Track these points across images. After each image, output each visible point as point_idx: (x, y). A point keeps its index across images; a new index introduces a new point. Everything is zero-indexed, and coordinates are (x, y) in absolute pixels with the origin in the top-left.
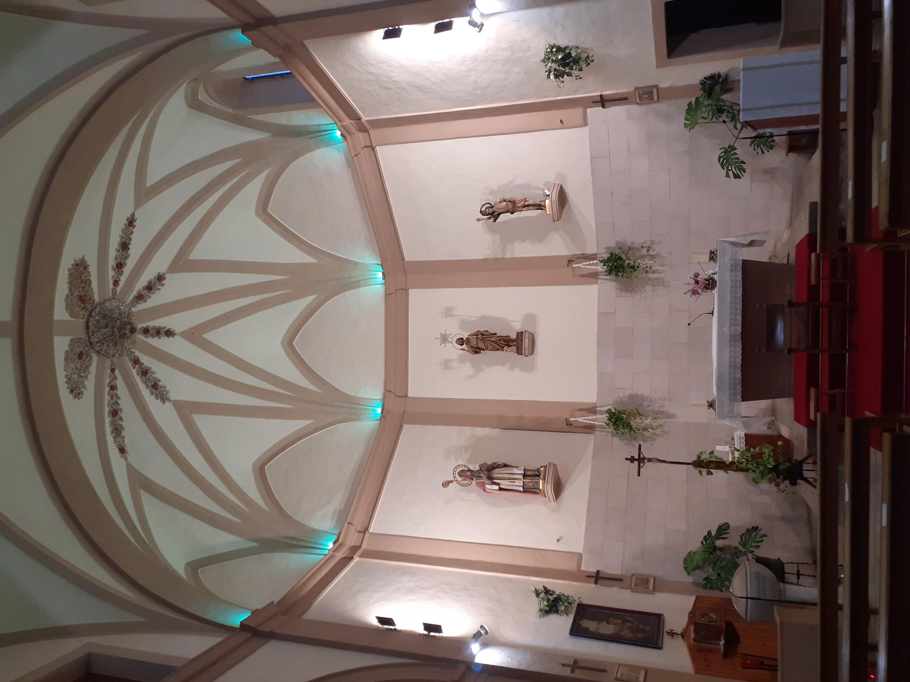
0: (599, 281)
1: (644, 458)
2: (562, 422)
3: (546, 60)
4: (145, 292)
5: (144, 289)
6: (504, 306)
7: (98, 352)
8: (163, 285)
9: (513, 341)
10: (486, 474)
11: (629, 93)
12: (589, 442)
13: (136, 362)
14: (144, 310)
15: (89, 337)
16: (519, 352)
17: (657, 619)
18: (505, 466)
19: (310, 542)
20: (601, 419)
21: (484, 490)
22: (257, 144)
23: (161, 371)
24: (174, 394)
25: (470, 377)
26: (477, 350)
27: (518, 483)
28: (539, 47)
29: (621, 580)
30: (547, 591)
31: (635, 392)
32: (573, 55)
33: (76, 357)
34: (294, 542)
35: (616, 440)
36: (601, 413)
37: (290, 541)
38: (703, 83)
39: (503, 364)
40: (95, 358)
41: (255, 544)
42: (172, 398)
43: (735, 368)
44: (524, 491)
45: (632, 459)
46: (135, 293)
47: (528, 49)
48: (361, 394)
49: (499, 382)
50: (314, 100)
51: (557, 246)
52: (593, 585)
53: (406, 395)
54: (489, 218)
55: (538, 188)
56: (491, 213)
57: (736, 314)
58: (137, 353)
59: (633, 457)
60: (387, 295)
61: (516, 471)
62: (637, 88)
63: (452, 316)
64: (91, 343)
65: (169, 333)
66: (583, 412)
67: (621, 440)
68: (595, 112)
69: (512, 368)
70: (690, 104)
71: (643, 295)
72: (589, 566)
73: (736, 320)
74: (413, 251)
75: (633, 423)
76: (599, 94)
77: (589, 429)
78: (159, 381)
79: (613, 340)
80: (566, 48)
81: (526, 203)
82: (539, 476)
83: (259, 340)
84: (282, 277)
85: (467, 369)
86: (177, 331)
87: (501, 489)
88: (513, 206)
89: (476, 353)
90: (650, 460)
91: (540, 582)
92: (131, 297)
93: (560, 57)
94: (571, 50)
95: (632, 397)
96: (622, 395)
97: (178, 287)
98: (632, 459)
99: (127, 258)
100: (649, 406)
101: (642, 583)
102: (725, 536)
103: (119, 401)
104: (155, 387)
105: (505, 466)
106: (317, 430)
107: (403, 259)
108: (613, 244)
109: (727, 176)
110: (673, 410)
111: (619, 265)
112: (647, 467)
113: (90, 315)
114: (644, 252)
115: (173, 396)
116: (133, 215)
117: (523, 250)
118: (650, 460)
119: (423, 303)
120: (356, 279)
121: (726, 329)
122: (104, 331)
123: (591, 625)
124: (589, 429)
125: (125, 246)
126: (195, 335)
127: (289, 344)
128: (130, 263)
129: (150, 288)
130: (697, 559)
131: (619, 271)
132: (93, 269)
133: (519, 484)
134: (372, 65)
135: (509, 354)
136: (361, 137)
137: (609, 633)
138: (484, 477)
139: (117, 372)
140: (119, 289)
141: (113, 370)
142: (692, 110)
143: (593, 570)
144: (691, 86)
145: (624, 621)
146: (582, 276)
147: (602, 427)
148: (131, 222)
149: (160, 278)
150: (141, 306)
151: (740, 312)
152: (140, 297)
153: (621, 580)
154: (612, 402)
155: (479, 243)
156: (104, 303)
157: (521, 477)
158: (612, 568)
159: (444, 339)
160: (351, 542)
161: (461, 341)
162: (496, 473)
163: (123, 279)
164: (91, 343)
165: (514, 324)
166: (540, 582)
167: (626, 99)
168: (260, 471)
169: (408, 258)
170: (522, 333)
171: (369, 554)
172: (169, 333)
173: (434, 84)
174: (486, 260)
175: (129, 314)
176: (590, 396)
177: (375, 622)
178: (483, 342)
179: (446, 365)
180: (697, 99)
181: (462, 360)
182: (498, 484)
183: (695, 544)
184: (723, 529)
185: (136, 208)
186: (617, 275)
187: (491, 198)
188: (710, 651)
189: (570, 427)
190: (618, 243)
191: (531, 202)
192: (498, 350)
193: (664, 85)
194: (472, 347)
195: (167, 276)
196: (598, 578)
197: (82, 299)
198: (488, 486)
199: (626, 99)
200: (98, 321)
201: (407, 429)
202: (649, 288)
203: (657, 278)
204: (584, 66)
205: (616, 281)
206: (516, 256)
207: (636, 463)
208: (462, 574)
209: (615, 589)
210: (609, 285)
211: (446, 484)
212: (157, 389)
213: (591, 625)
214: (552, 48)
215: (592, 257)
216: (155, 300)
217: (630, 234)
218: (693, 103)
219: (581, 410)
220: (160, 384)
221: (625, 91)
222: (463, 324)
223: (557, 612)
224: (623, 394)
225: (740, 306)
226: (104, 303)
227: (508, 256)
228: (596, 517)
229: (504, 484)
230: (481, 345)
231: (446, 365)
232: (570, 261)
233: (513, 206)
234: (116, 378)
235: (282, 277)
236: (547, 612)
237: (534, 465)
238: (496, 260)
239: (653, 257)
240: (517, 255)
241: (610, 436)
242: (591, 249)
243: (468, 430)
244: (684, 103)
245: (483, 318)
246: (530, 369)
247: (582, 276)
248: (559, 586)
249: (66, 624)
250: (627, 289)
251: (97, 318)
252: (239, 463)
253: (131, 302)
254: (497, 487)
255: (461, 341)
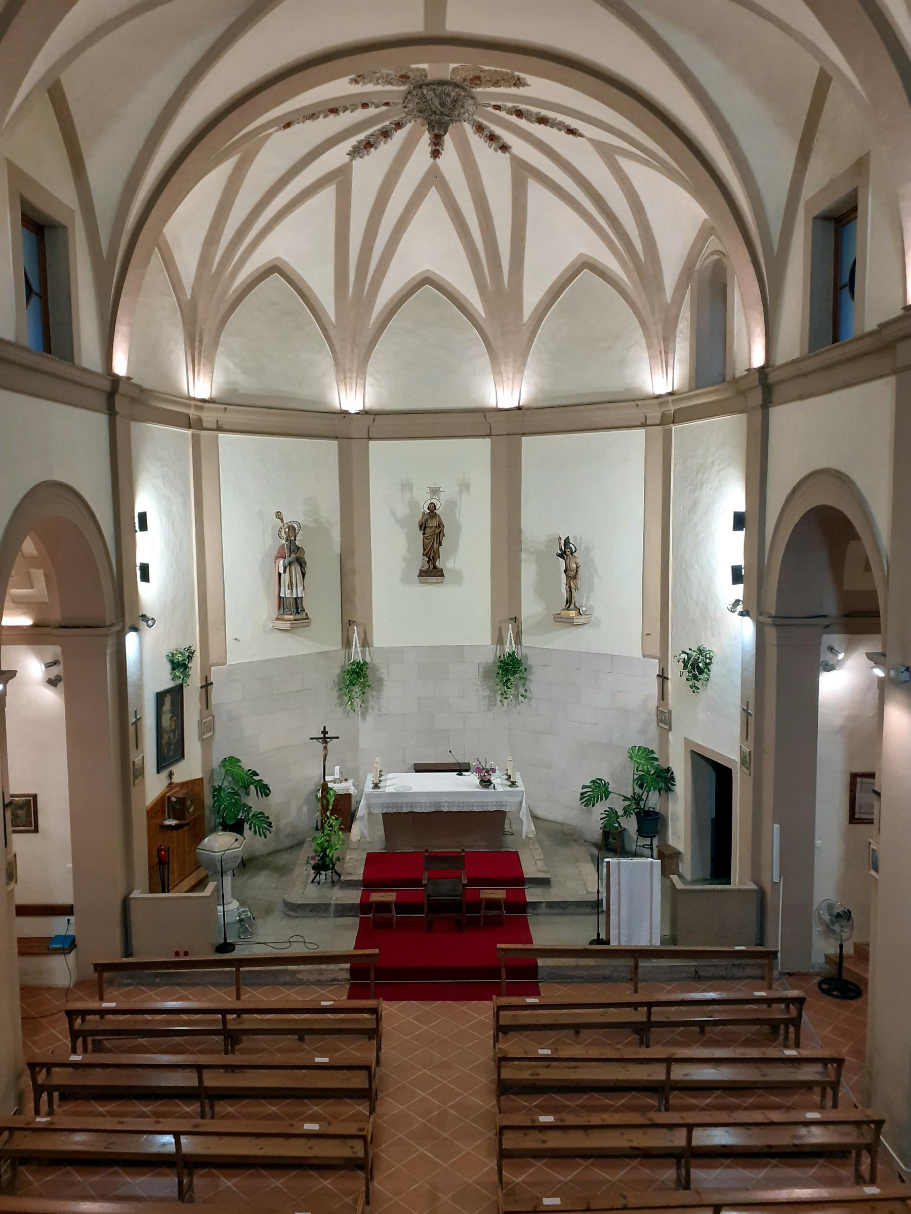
0: (494, 646)
1: (326, 743)
2: (352, 619)
3: (700, 651)
4: (486, 132)
5: (491, 131)
6: (471, 549)
7: (409, 93)
8: (496, 150)
9: (434, 564)
10: (293, 555)
11: (667, 704)
12: (334, 644)
13: (399, 125)
14: (464, 131)
15: (427, 85)
16: (423, 573)
17: (180, 754)
18: (303, 574)
19: (199, 365)
20: (357, 653)
21: (277, 558)
22: (660, 288)
23: (388, 150)
24: (359, 164)
25: (394, 515)
26: (423, 527)
27: (288, 592)
28: (714, 646)
29: (207, 707)
30: (190, 658)
31: (385, 683)
32: (701, 677)
33: (403, 73)
34: (197, 344)
35: (337, 671)
36: (363, 653)
37: (197, 339)
38: (668, 770)
39: (408, 551)
40: (403, 88)
41: (189, 297)
42: (354, 162)
43: (411, 807)
44: (280, 597)
45: (325, 732)
46: (485, 123)
47: (713, 635)
48: (369, 379)
49: (390, 548)
50: (697, 388)
51: (531, 608)
52: (199, 685)
53: (370, 439)
54: (561, 549)
55: (588, 598)
56: (566, 551)
57: (459, 806)
58: (409, 126)
59: (327, 733)
60: (485, 412)
61: (300, 589)
62: (670, 712)
63: (461, 491)
64: (420, 87)
65: (436, 154)
66: (363, 634)
67: (338, 675)
68: (654, 667)
69: (406, 560)
70: (653, 752)
71: (480, 688)
72: (215, 674)
73: (453, 806)
74: (534, 449)
75: (357, 689)
76: (670, 677)
77: (347, 643)
78: (376, 148)
79: (436, 661)
80: (709, 670)
81: (573, 590)
82: (297, 612)
83: (430, 247)
84: (506, 281)
85: (403, 510)
86: (438, 161)
87: (280, 574)
88: (572, 575)
89: (421, 526)
90: (325, 748)
91: (197, 648)
92: (480, 120)
93: (701, 665)
94: (707, 674)
95: (381, 681)
96: (382, 671)
97: (494, 168)
98: (325, 732)
99: (529, 120)
100: (373, 696)
101: (207, 728)
102: (259, 794)
103: (348, 112)
104: (368, 145)
105: (303, 574)
106: (324, 330)
107: (524, 434)
108: (530, 662)
109: (584, 787)
110: (370, 718)
111: (509, 670)
112: (319, 745)
113: (456, 85)
114: (522, 691)
115: (357, 163)
116: (581, 135)
117: (529, 573)
118: (325, 748)
119: (476, 454)
120: (503, 370)
121: (445, 799)
122: (437, 102)
123: (167, 706)
124: (347, 643)
125: (543, 120)
126: (434, 178)
127: (427, 280)
128: (522, 123)
129: (492, 138)
130: (236, 770)
131: (503, 671)
132: (513, 90)
133: (286, 593)
134: (719, 471)
135: (420, 562)
136: (655, 415)
137: (163, 724)
138: (291, 559)
139: (384, 108)
140: (490, 109)
141: (387, 104)
142: (648, 754)
143: (212, 679)
144: (668, 759)
145: (174, 731)
146: (500, 630)
147: (350, 654)
148: (571, 131)
149: (504, 148)
150: (468, 128)
151: (461, 810)
152: (480, 128)
153: (207, 707)
154: (375, 662)
155: (539, 525)
156: (473, 98)
157: (295, 596)
158: (215, 695)
159: (435, 491)
160: (209, 417)
161: (432, 508)
162: (296, 568)
163: (503, 114)
164: (420, 87)
165: (452, 561)
166: (197, 648)
167: (663, 700)
168: (274, 269)
169: (527, 441)
170: (442, 575)
171: (196, 441)
172: (436, 154)
173: (696, 524)
174: (519, 531)
175: (459, 119)
176: (379, 640)
177: (138, 509)
178: (432, 531)
179: (407, 486)
180: (656, 759)
181: (413, 504)
182: (285, 572)
183: (247, 764)
184: (264, 790)
185: (590, 140)
186: (500, 667)
187: (583, 549)
188: (163, 812)
189: (347, 624)
190: (531, 667)
191: (574, 594)
192: (424, 550)
193: (671, 736)
194: (426, 521)
195: (507, 155)
196: (207, 686)
197: (478, 78)
198: (282, 562)
199: (663, 700)
200: (448, 95)
201: (332, 446)
202: (487, 693)
203: (496, 699)
204: (690, 683)
205: (494, 662)
206: (522, 564)
207: (322, 736)
208: (192, 554)
209: (199, 705)
210: (489, 655)
211: (279, 515)
212: (365, 147)
213: (167, 706)
214: (710, 659)
215: (518, 641)
216: (477, 143)
217: (539, 679)
218: (654, 755)
219: (365, 632)
220: (373, 149)
221: (670, 701)
222: (452, 505)
223: (173, 669)
224: (383, 672)
225: (465, 810)
226: (473, 98)
227: (523, 556)
228: (265, 672)
229: (285, 578)
230: (428, 530)
231: (407, 486)
232: (515, 620)
233: (572, 575)
234: (377, 107)
235: (506, 281)
236: (172, 662)
237: (306, 605)
238: (520, 542)
239: (517, 697)
240: (523, 565)
241: (341, 664)
242: (525, 640)
243: (337, 517)
244: (654, 747)
245: (458, 528)
246: (405, 580)
247: (500, 630)
248: (195, 666)
249: (87, 166)
250: (486, 674)
251: (453, 94)
252: (278, 246)
253: (475, 121)
254: (281, 571)
255: (432, 508)
